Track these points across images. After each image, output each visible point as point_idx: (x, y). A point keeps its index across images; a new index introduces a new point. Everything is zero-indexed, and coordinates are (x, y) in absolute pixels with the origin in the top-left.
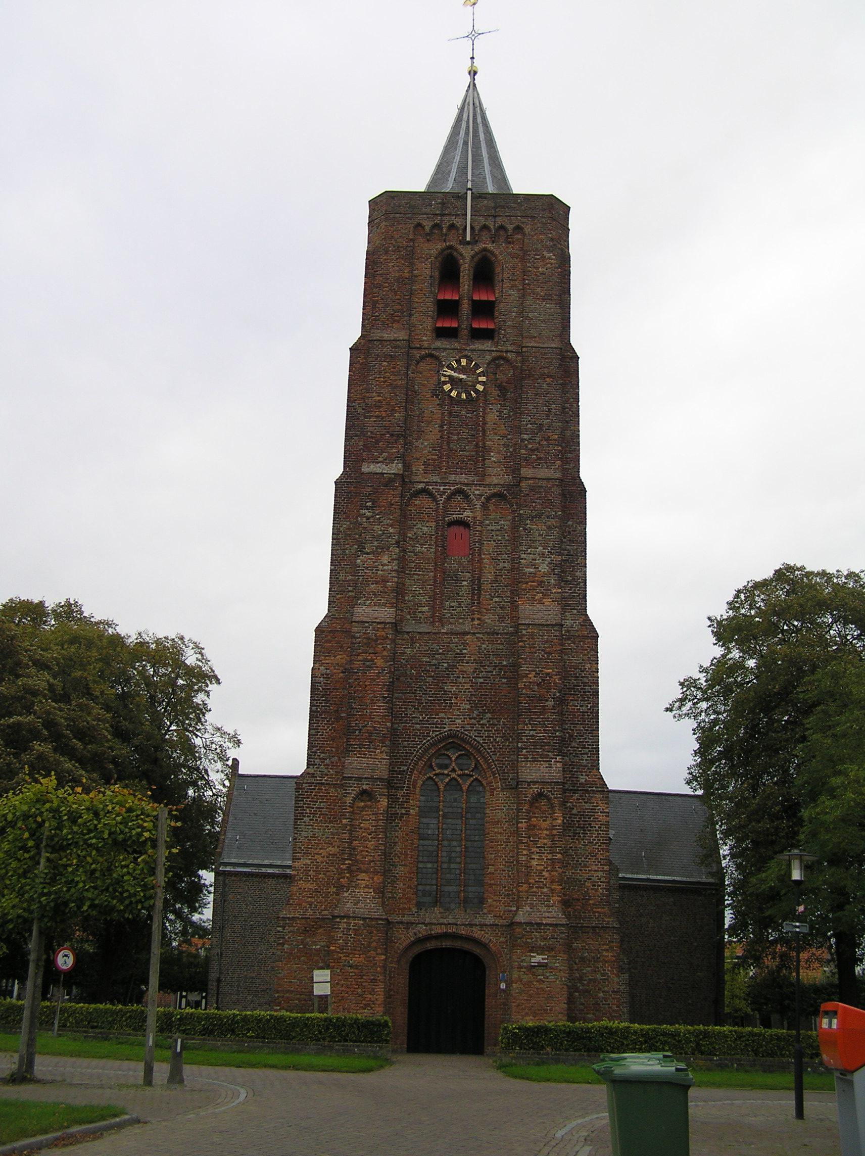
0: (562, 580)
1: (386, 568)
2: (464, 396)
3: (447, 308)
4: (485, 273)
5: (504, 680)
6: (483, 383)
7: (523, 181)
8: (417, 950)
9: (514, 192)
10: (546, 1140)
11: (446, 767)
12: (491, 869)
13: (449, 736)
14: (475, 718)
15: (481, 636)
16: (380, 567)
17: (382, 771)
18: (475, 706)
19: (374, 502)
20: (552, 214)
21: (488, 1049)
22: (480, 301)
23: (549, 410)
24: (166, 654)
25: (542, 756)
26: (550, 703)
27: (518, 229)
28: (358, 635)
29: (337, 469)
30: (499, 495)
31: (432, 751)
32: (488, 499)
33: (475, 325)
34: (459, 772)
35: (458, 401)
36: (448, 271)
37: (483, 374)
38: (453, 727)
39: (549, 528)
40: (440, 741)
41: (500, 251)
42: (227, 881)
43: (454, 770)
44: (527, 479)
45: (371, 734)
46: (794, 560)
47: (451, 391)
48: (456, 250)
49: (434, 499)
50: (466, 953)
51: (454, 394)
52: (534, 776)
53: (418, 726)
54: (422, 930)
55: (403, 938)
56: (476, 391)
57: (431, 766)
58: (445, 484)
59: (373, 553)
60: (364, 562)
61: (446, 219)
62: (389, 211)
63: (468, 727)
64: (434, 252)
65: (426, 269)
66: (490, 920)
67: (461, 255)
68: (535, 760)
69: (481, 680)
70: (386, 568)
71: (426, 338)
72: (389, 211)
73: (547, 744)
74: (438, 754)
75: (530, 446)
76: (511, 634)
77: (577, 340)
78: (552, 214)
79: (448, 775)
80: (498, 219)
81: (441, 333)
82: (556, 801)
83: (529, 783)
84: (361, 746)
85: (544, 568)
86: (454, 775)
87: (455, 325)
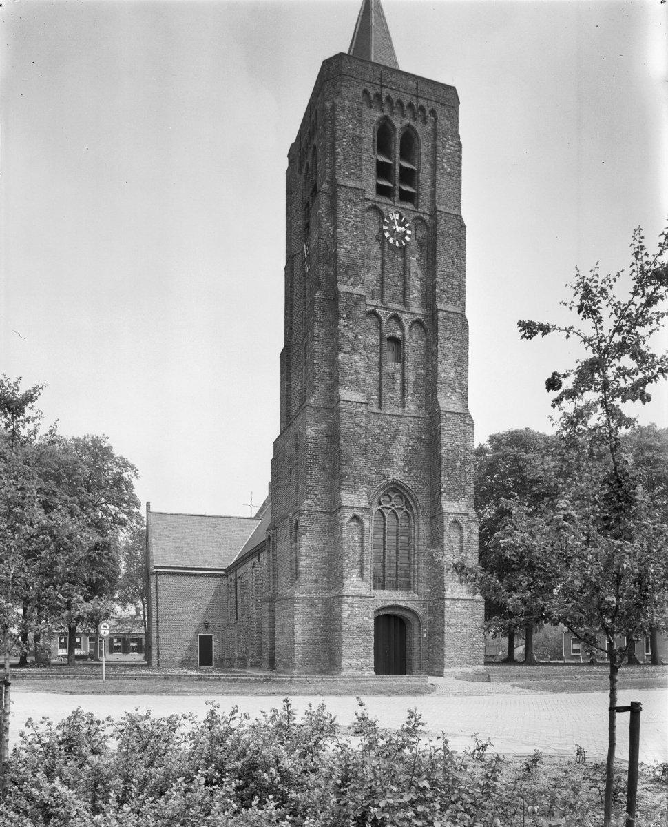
1: (357, 364)
2: (397, 244)
3: (383, 170)
5: (423, 449)
6: (410, 236)
10: (266, 654)
13: (393, 483)
14: (407, 472)
15: (410, 418)
16: (354, 363)
19: (348, 315)
23: (453, 262)
24: (81, 445)
25: (454, 497)
26: (459, 464)
27: (433, 112)
28: (344, 410)
30: (418, 322)
31: (382, 493)
32: (413, 323)
33: (380, 182)
34: (396, 507)
35: (392, 247)
36: (383, 143)
37: (409, 228)
38: (395, 477)
39: (455, 347)
40: (386, 486)
41: (422, 130)
42: (159, 578)
43: (393, 505)
44: (442, 310)
45: (355, 478)
46: (494, 432)
47: (389, 237)
52: (452, 510)
53: (374, 476)
54: (381, 604)
56: (405, 241)
58: (386, 309)
59: (349, 352)
60: (343, 359)
61: (385, 91)
63: (403, 478)
64: (376, 119)
65: (369, 134)
67: (393, 126)
68: (449, 500)
69: (410, 448)
70: (357, 364)
71: (372, 193)
73: (457, 490)
75: (442, 288)
79: (389, 508)
80: (419, 100)
82: (464, 526)
83: (449, 514)
86: (393, 508)
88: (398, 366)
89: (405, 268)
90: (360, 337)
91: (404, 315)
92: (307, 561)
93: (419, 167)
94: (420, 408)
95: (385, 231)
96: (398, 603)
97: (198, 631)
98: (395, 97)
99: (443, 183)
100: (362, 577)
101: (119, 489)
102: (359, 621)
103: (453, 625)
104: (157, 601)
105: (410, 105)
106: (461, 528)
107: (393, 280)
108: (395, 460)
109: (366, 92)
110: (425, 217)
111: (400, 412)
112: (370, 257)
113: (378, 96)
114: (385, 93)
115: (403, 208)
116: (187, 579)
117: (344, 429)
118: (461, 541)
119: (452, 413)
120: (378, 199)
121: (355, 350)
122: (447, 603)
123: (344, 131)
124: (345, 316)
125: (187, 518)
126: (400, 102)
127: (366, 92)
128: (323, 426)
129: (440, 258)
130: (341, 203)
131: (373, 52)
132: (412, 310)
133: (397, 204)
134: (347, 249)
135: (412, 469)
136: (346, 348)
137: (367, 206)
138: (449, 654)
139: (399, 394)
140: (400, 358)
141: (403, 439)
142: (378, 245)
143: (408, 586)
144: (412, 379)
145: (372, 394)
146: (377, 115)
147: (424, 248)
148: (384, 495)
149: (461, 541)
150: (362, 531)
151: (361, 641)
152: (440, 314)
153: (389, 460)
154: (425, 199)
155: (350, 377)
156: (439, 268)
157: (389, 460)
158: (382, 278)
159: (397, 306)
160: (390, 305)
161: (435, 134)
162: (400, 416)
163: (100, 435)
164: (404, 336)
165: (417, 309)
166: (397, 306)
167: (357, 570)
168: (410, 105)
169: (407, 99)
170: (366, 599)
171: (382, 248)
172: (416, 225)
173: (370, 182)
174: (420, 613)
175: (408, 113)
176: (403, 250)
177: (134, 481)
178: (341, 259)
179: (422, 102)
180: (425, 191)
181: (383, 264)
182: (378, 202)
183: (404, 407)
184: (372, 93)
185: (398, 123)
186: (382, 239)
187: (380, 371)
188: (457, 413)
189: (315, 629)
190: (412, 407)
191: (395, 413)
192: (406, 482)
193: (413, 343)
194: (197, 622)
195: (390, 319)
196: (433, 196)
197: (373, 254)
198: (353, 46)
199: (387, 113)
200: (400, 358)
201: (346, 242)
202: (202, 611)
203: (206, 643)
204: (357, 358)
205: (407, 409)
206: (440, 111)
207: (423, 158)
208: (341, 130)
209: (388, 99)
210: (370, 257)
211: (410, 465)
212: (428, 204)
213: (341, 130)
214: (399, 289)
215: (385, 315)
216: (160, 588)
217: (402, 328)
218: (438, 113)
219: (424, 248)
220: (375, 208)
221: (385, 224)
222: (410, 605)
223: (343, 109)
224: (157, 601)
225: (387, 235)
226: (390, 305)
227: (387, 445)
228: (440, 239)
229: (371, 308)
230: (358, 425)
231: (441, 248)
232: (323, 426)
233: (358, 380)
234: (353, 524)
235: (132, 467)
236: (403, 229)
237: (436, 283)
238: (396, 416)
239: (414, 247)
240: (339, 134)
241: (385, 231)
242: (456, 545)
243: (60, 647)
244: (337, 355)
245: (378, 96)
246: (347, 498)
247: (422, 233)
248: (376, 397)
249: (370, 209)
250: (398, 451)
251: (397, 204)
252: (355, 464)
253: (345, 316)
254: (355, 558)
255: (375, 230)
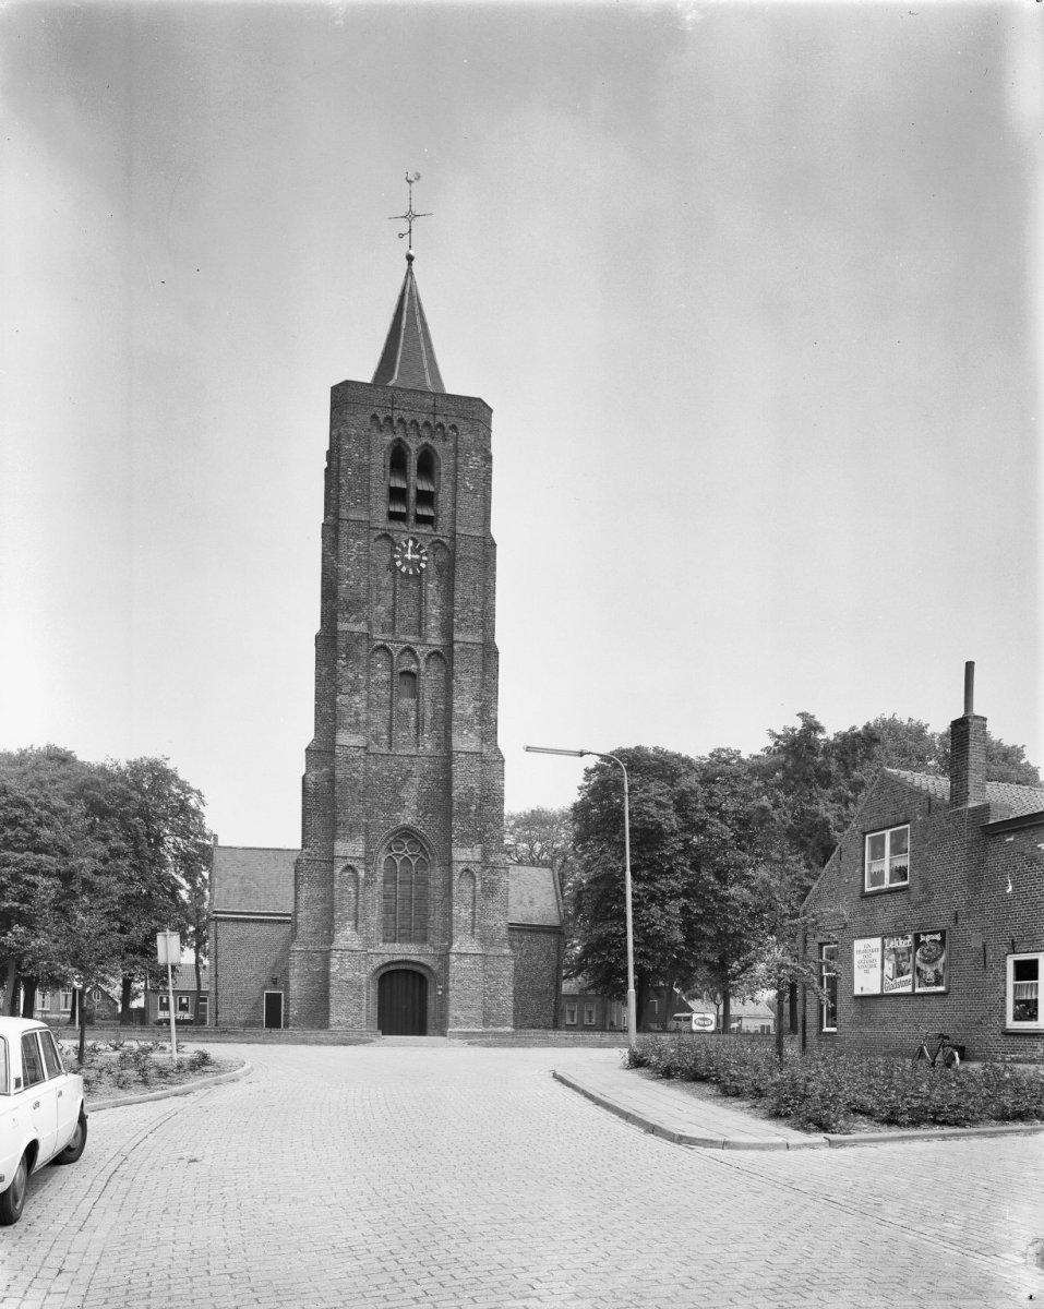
0: (482, 722)
2: (411, 572)
3: (397, 495)
4: (427, 466)
6: (426, 562)
7: (455, 383)
8: (379, 975)
9: (449, 390)
11: (400, 849)
12: (432, 918)
17: (478, 857)
18: (420, 808)
20: (475, 413)
21: (429, 1031)
22: (396, 488)
24: (137, 769)
26: (473, 808)
27: (454, 427)
29: (317, 627)
30: (436, 653)
31: (391, 839)
32: (429, 656)
33: (392, 509)
35: (406, 575)
36: (398, 462)
39: (474, 681)
41: (439, 446)
43: (406, 852)
44: (458, 642)
47: (401, 566)
48: (404, 443)
49: (390, 654)
50: (414, 972)
51: (404, 569)
52: (464, 858)
54: (388, 959)
55: (377, 962)
57: (391, 849)
62: (344, 397)
64: (387, 443)
65: (380, 459)
66: (431, 951)
67: (408, 447)
68: (462, 847)
71: (382, 522)
72: (344, 397)
73: (471, 836)
74: (396, 841)
76: (446, 757)
77: (496, 530)
78: (475, 413)
80: (438, 417)
81: (393, 516)
82: (477, 875)
84: (344, 835)
85: (470, 711)
87: (404, 510)
88: (412, 702)
89: (421, 600)
90: (361, 677)
91: (418, 647)
92: (305, 913)
93: (438, 489)
94: (438, 745)
95: (396, 560)
96: (408, 958)
97: (265, 988)
98: (408, 417)
99: (466, 504)
100: (356, 929)
101: (185, 814)
102: (349, 976)
103: (459, 981)
104: (216, 952)
105: (427, 424)
106: (473, 877)
107: (408, 611)
108: (406, 803)
109: (374, 417)
110: (444, 540)
111: (413, 752)
112: (379, 588)
113: (389, 419)
114: (396, 415)
115: (418, 533)
116: (253, 925)
117: (339, 775)
118: (474, 891)
119: (466, 753)
120: (390, 526)
121: (355, 691)
122: (453, 957)
123: (349, 461)
124: (344, 656)
125: (261, 853)
126: (414, 422)
127: (374, 417)
128: (324, 770)
129: (459, 585)
130: (343, 538)
131: (399, 360)
132: (429, 641)
133: (411, 530)
134: (347, 585)
135: (426, 813)
136: (346, 689)
137: (376, 535)
138: (454, 1012)
139: (413, 732)
140: (415, 694)
141: (417, 781)
142: (390, 574)
143: (424, 940)
144: (429, 715)
145: (381, 734)
146: (389, 438)
147: (445, 573)
148: (396, 841)
149: (474, 891)
150: (357, 881)
151: (351, 997)
152: (456, 647)
153: (401, 805)
154: (444, 520)
155: (349, 720)
156: (457, 595)
157: (401, 805)
158: (394, 611)
159: (411, 638)
160: (403, 637)
161: (456, 450)
162: (412, 756)
163: (159, 758)
164: (419, 670)
165: (435, 640)
166: (411, 638)
167: (351, 923)
168: (427, 424)
169: (422, 418)
170: (358, 954)
171: (394, 577)
172: (436, 549)
173: (381, 507)
174: (435, 969)
175: (425, 432)
176: (418, 578)
177: (203, 809)
178: (342, 595)
179: (440, 419)
180: (445, 512)
181: (395, 593)
182: (389, 530)
183: (418, 746)
184: (382, 417)
185: (413, 445)
186: (392, 567)
187: (391, 708)
188: (472, 753)
189: (313, 983)
190: (429, 746)
191: (406, 752)
192: (419, 828)
193: (430, 678)
194: (264, 977)
195: (402, 653)
196: (454, 516)
197: (384, 584)
198: (418, 319)
199: (400, 435)
200: (415, 694)
201: (348, 577)
202: (270, 964)
203: (273, 1003)
204: (357, 699)
205: (421, 748)
206: (462, 425)
207: (443, 478)
208: (346, 460)
209: (401, 420)
210: (379, 588)
211: (424, 808)
212: (448, 526)
213: (346, 460)
214: (413, 620)
215: (396, 649)
216: (220, 935)
217: (417, 661)
218: (460, 428)
219: (445, 573)
220: (386, 536)
221: (396, 552)
222: (423, 960)
223: (349, 437)
224: (216, 952)
225: (399, 563)
226: (403, 637)
227: (396, 788)
228: (459, 565)
229: (379, 643)
230: (355, 770)
231: (460, 572)
232: (324, 770)
233: (358, 723)
234: (347, 874)
235: (199, 793)
236: (417, 557)
237: (454, 611)
238: (407, 756)
239: (432, 573)
240: (343, 464)
241: (396, 560)
242: (468, 895)
243: (162, 1009)
244: (335, 696)
245: (389, 419)
246: (341, 848)
247: (442, 557)
248: (385, 737)
249: (379, 537)
250: (410, 794)
251: (411, 530)
252: (353, 810)
253: (344, 656)
254: (349, 910)
255: (386, 558)
